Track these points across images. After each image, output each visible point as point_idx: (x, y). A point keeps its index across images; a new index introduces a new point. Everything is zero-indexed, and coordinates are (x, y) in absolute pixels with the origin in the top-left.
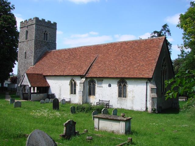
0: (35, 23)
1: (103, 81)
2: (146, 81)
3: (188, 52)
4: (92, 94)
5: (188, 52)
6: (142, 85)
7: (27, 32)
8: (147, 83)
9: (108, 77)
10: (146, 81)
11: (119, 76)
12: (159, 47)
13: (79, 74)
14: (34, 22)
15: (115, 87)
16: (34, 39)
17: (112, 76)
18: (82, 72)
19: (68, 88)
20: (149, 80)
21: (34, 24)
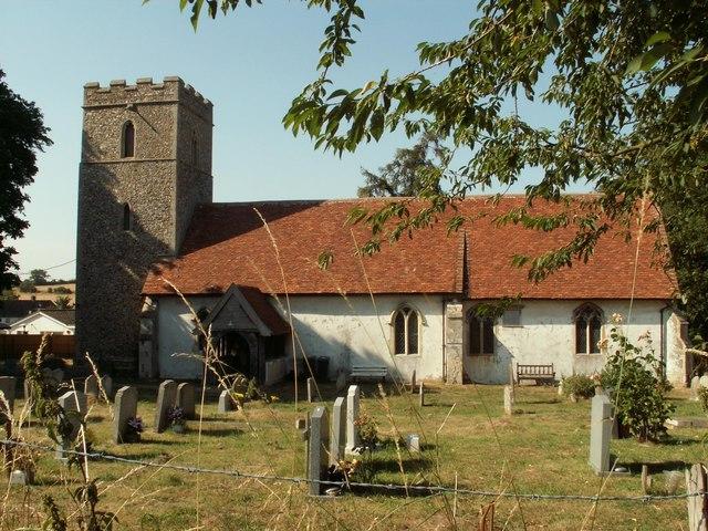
0: (175, 98)
1: (523, 311)
2: (659, 308)
3: (158, 273)
4: (482, 350)
5: (158, 273)
6: (649, 312)
7: (128, 128)
8: (662, 311)
9: (550, 299)
10: (659, 308)
11: (578, 295)
12: (278, 423)
13: (437, 290)
14: (173, 94)
15: (568, 331)
16: (174, 156)
17: (560, 296)
18: (449, 279)
19: (389, 333)
20: (667, 306)
21: (174, 102)
